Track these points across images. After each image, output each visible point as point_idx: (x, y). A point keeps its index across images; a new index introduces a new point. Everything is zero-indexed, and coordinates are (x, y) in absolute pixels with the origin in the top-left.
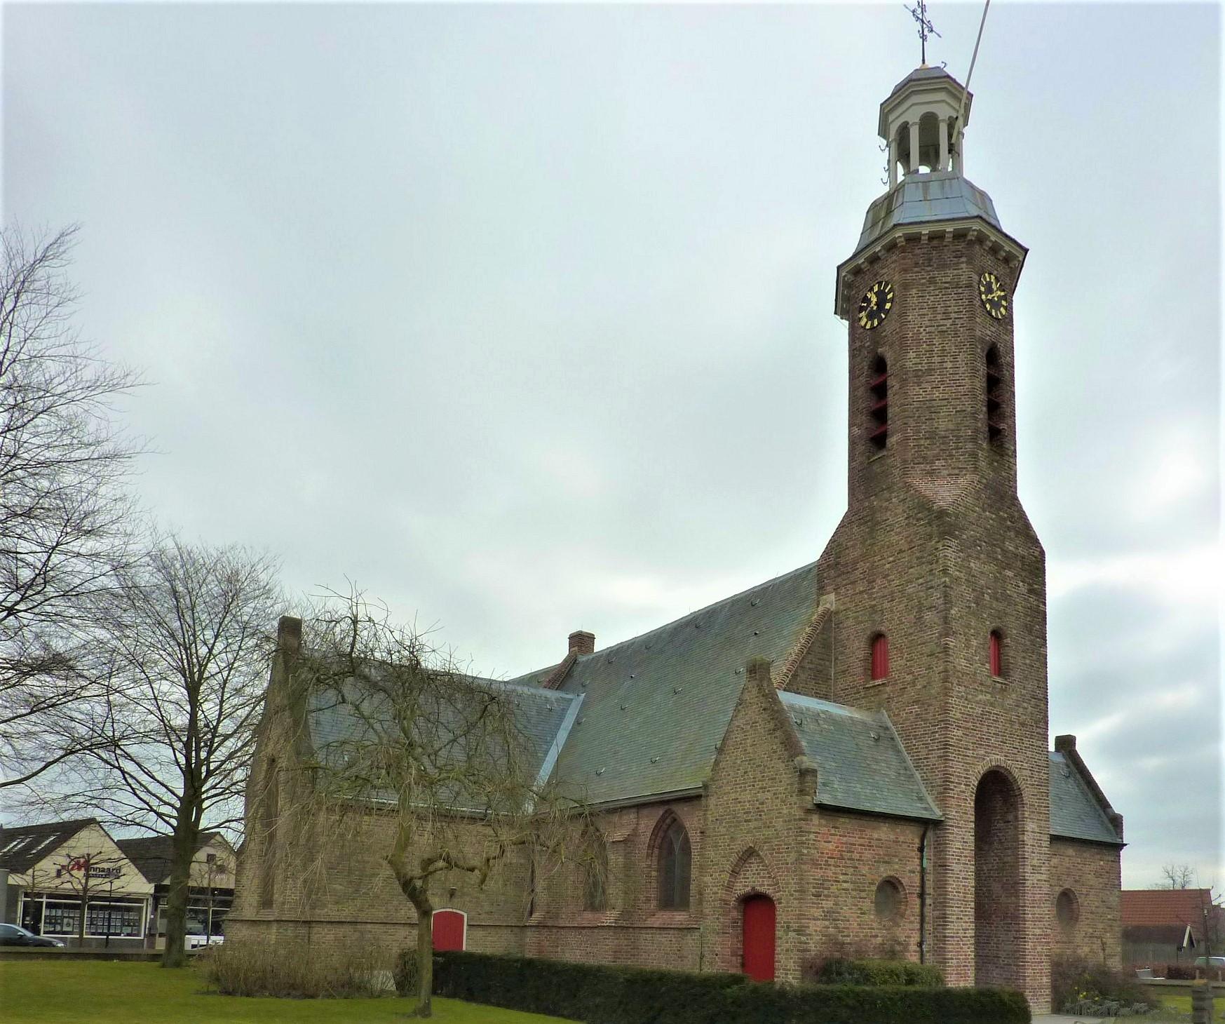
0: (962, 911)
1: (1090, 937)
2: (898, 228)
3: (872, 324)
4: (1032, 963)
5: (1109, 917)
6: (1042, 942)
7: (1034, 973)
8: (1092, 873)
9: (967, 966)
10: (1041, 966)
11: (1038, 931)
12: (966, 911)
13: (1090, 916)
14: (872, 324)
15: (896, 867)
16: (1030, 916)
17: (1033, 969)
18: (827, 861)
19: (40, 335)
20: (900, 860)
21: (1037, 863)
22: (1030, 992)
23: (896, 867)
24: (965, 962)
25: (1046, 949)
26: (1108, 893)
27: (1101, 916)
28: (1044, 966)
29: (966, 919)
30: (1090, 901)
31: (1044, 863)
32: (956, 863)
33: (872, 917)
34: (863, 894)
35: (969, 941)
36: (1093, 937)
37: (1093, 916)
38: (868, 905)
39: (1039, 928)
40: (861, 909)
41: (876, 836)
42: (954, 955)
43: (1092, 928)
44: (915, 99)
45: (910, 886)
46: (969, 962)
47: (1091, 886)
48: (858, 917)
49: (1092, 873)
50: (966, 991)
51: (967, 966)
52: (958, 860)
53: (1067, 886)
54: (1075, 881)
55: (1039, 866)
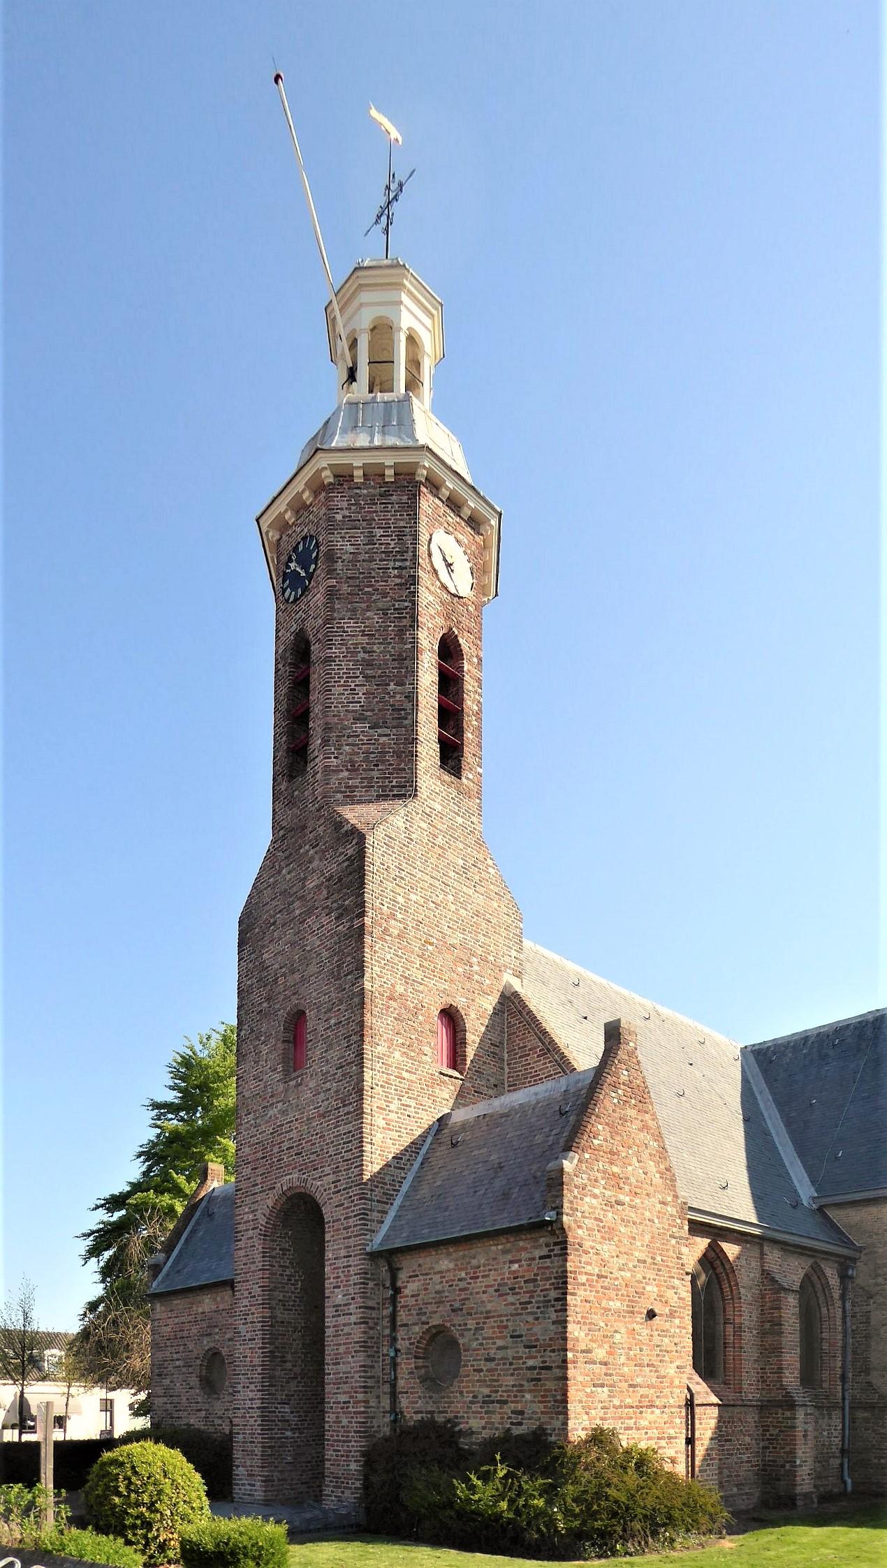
0: (248, 1379)
1: (484, 1402)
2: (364, 289)
3: (296, 594)
4: (335, 1441)
5: (531, 1363)
6: (350, 1413)
7: (337, 1456)
8: (491, 1290)
9: (254, 1442)
10: (348, 1446)
11: (343, 1398)
12: (252, 1378)
13: (485, 1366)
14: (296, 594)
15: (217, 1337)
16: (331, 1376)
17: (334, 1451)
18: (532, 1297)
19: (422, 712)
20: (220, 1330)
21: (342, 1300)
22: (331, 1481)
23: (217, 1337)
24: (252, 1438)
25: (356, 1422)
26: (530, 1319)
27: (511, 1364)
28: (353, 1446)
29: (252, 1387)
30: (484, 1339)
31: (353, 1299)
32: (243, 1324)
33: (197, 1391)
34: (191, 1370)
35: (255, 1413)
36: (493, 1402)
37: (492, 1365)
38: (194, 1381)
39: (344, 1393)
40: (189, 1384)
41: (200, 1310)
42: (241, 1429)
43: (488, 1386)
44: (365, 297)
45: (228, 1355)
46: (256, 1438)
47: (487, 1312)
48: (187, 1392)
49: (491, 1290)
50: (97, 1440)
51: (254, 1442)
52: (246, 1319)
53: (435, 1321)
54: (453, 1310)
55: (345, 1305)
